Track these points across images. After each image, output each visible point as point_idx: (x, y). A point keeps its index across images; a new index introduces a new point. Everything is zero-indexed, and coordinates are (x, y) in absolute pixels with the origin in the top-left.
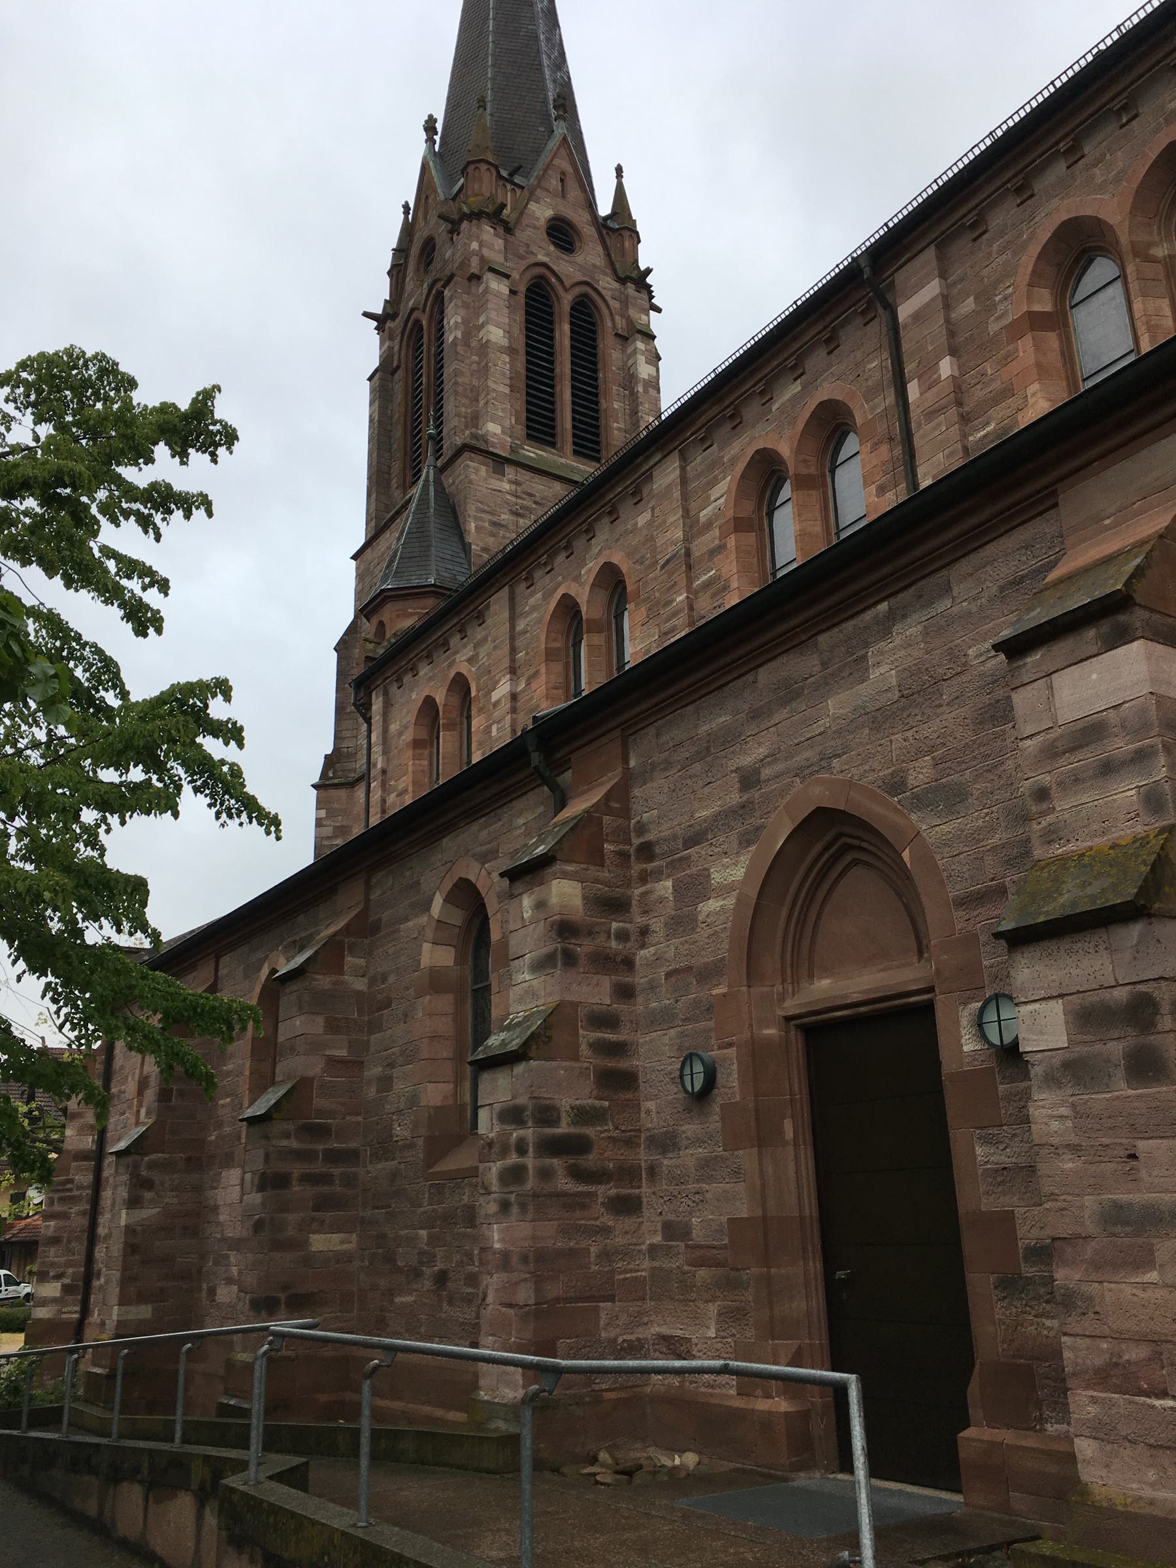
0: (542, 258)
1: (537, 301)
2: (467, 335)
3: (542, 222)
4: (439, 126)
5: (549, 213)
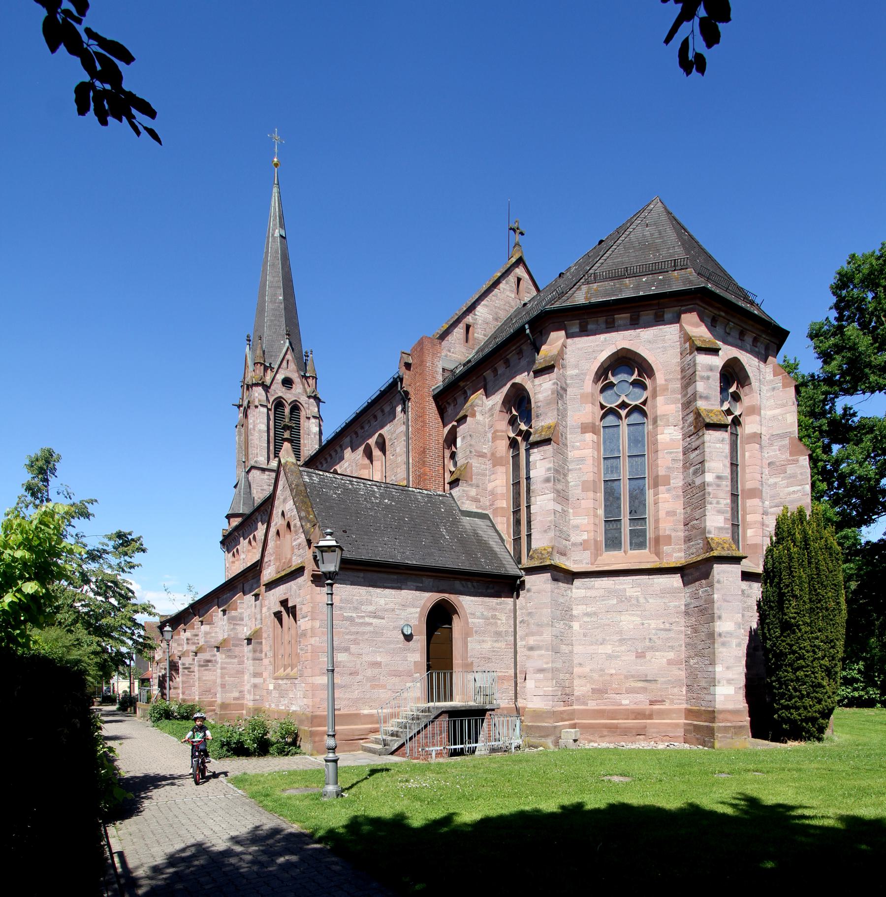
0: (280, 394)
1: (279, 404)
2: (254, 426)
3: (280, 381)
4: (251, 338)
5: (283, 377)
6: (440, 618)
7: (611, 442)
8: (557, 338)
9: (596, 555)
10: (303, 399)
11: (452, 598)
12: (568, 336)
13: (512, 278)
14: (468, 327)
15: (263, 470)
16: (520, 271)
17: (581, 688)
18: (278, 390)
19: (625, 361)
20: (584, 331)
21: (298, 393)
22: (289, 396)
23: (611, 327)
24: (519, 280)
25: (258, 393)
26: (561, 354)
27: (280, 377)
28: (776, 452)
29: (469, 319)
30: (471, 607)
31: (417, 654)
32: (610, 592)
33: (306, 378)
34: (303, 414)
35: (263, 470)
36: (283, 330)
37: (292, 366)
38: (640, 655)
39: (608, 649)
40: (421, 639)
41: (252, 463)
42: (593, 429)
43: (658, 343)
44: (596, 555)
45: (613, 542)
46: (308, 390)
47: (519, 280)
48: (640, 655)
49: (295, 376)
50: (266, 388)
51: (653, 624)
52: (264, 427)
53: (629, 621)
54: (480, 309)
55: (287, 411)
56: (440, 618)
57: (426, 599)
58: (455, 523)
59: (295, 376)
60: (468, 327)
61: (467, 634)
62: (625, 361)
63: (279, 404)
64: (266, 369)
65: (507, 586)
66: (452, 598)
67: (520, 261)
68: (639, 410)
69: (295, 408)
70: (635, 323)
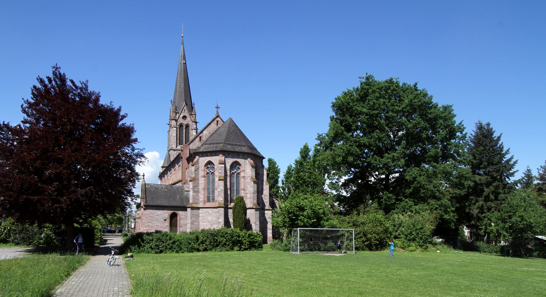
0: (181, 122)
6: (173, 217)
7: (209, 180)
8: (197, 157)
9: (204, 204)
10: (190, 123)
11: (176, 212)
12: (200, 157)
13: (215, 122)
14: (200, 137)
15: (175, 150)
16: (218, 119)
17: (430, 246)
18: (181, 121)
19: (210, 163)
20: (203, 156)
21: (188, 121)
22: (185, 122)
23: (207, 156)
24: (217, 121)
25: (173, 123)
26: (197, 161)
27: (181, 116)
28: (248, 180)
29: (201, 135)
30: (180, 213)
31: (167, 223)
32: (207, 212)
33: (192, 115)
34: (190, 128)
35: (175, 150)
36: (183, 98)
37: (186, 111)
38: (212, 225)
39: (206, 224)
40: (168, 221)
41: (170, 148)
42: (204, 177)
43: (216, 159)
44: (204, 204)
45: (209, 201)
46: (193, 119)
47: (217, 121)
48: (212, 225)
49: (187, 115)
50: (176, 121)
51: (214, 219)
52: (175, 135)
53: (209, 218)
54: (204, 132)
55: (184, 127)
56: (173, 217)
57: (170, 212)
58: (183, 193)
59: (187, 115)
60: (200, 137)
61: (180, 219)
62: (210, 163)
63: (181, 125)
64: (176, 113)
65: (184, 209)
66: (176, 212)
67: (218, 116)
68: (212, 173)
69: (187, 126)
70: (212, 155)
